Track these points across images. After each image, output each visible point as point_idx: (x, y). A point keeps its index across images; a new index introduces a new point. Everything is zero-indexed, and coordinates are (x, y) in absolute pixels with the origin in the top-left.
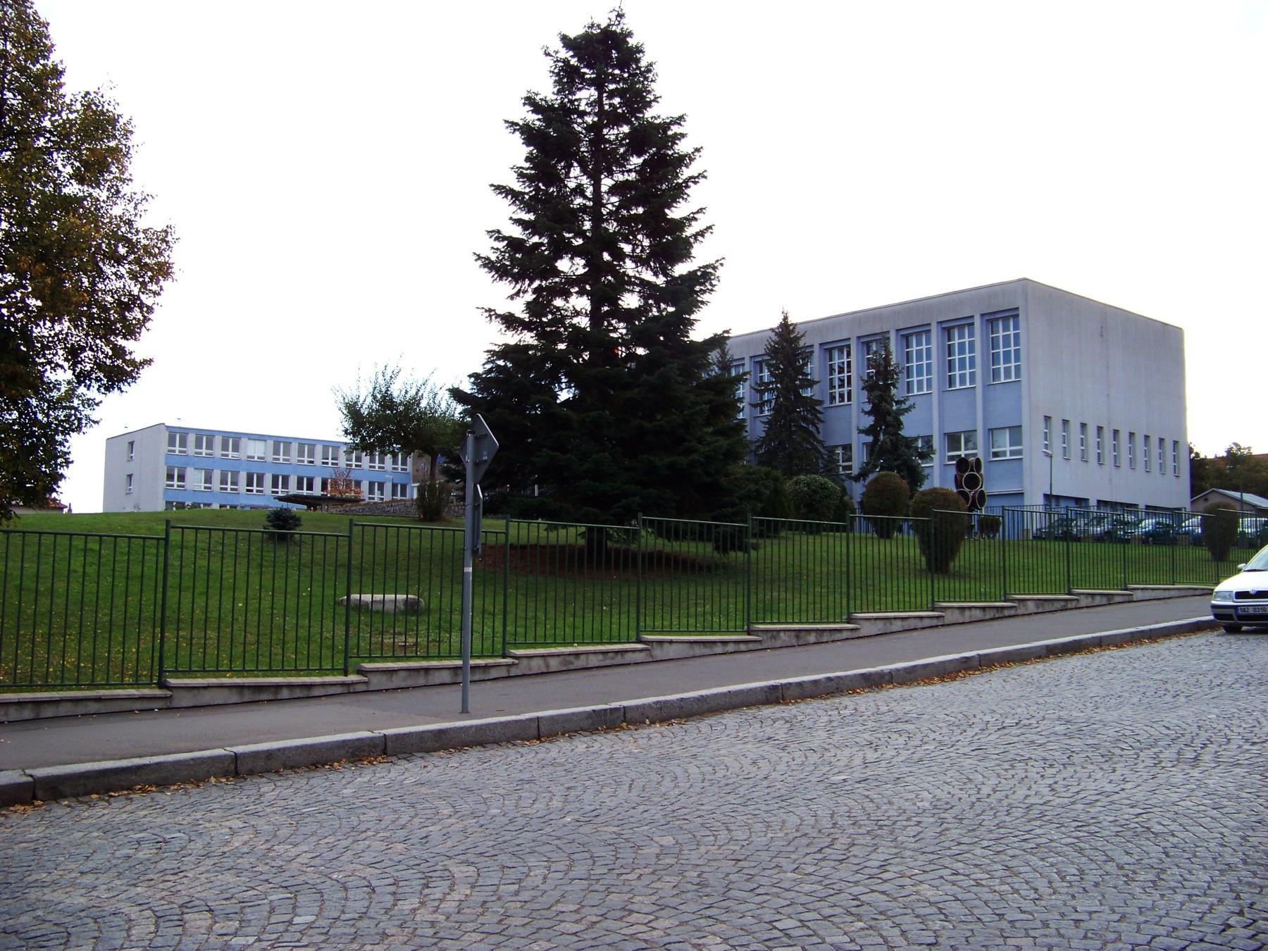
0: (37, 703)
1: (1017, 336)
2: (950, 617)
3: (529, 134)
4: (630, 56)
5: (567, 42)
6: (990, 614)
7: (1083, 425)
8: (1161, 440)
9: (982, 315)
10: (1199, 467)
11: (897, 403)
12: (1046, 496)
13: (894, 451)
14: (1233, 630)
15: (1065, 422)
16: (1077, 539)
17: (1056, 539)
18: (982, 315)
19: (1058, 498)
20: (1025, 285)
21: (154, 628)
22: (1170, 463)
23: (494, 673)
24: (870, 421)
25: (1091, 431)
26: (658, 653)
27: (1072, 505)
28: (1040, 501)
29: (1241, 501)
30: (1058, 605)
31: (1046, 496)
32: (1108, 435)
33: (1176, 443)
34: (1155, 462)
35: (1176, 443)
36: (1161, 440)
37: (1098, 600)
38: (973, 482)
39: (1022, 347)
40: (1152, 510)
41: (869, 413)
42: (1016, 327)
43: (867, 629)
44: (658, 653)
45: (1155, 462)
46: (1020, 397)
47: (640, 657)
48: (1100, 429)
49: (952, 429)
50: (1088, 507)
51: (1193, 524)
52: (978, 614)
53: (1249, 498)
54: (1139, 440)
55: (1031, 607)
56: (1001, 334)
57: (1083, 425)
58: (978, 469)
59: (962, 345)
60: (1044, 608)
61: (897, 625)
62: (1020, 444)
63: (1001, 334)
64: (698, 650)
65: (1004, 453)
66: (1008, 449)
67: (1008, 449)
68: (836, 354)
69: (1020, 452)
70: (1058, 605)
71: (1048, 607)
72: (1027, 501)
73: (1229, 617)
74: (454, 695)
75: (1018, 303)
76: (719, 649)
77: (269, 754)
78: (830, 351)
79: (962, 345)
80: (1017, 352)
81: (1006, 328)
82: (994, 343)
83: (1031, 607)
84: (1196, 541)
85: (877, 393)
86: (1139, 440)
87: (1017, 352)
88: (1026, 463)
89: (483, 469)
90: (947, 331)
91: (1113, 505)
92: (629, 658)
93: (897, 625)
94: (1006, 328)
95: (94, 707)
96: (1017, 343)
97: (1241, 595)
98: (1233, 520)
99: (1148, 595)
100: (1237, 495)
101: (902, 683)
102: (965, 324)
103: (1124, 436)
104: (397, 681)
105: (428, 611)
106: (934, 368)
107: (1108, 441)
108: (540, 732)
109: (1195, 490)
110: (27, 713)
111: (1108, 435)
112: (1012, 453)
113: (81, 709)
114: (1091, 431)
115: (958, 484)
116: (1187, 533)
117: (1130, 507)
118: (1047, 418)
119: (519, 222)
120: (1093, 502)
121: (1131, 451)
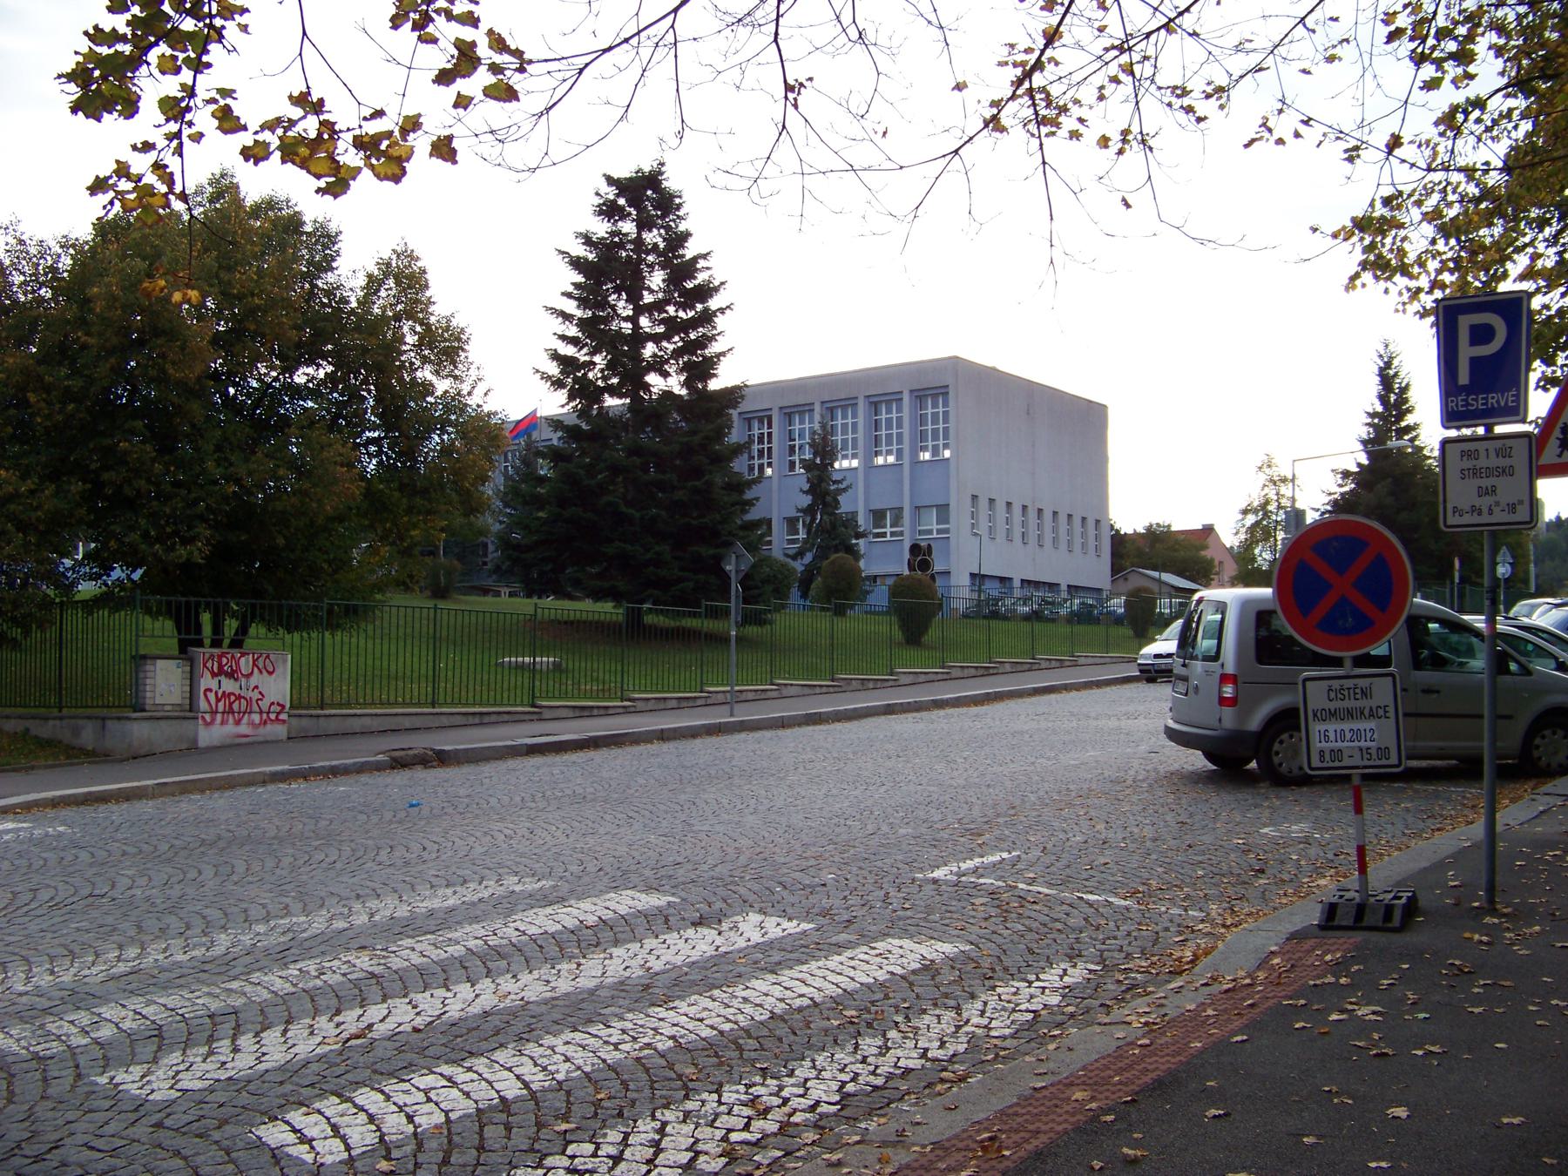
0: (481, 714)
1: (946, 414)
2: (956, 673)
3: (577, 263)
4: (668, 204)
5: (610, 180)
6: (981, 672)
7: (1009, 504)
8: (1084, 519)
9: (911, 391)
10: (1119, 541)
11: (835, 482)
12: (972, 575)
13: (830, 528)
14: (1151, 680)
15: (992, 501)
16: (1005, 618)
17: (985, 617)
18: (911, 391)
19: (984, 576)
20: (955, 364)
21: (128, 718)
22: (1092, 542)
23: (699, 702)
24: (806, 500)
25: (1017, 510)
26: (785, 692)
27: (997, 584)
28: (966, 581)
29: (1159, 581)
30: (1026, 667)
31: (972, 575)
32: (1032, 514)
33: (1098, 522)
34: (1078, 541)
35: (1098, 522)
36: (1084, 519)
37: (1054, 664)
38: (925, 565)
39: (951, 425)
40: (1073, 589)
41: (806, 492)
42: (946, 404)
43: (904, 680)
44: (785, 692)
45: (1078, 541)
46: (948, 477)
47: (774, 694)
48: (1024, 507)
49: (877, 506)
50: (1012, 588)
51: (1118, 604)
52: (973, 672)
53: (1168, 578)
54: (1063, 519)
55: (1008, 668)
56: (930, 411)
57: (1009, 504)
58: (930, 553)
59: (889, 421)
60: (1018, 668)
61: (922, 678)
62: (947, 522)
63: (930, 411)
64: (807, 691)
65: (930, 532)
66: (935, 527)
67: (935, 527)
68: (756, 424)
69: (947, 531)
70: (1026, 667)
71: (1019, 668)
72: (954, 581)
73: (1148, 671)
74: (727, 707)
75: (949, 381)
76: (818, 690)
77: (675, 730)
78: (749, 420)
79: (889, 421)
80: (946, 430)
81: (935, 405)
82: (923, 420)
83: (1008, 668)
84: (1118, 620)
85: (816, 473)
86: (1063, 519)
87: (946, 430)
88: (953, 541)
89: (741, 575)
90: (874, 405)
91: (1037, 584)
92: (770, 694)
93: (922, 678)
94: (935, 405)
95: (506, 717)
96: (946, 420)
97: (1157, 656)
98: (1152, 603)
99: (1090, 661)
100: (1155, 574)
101: (954, 706)
102: (894, 399)
103: (1048, 515)
104: (651, 705)
105: (567, 671)
106: (861, 443)
107: (1034, 520)
108: (783, 724)
109: (1116, 569)
110: (477, 720)
111: (1032, 514)
112: (939, 531)
113: (501, 718)
114: (1017, 510)
115: (911, 568)
116: (1109, 613)
117: (1053, 586)
118: (974, 497)
119: (563, 338)
120: (1064, 587)
121: (1055, 530)
